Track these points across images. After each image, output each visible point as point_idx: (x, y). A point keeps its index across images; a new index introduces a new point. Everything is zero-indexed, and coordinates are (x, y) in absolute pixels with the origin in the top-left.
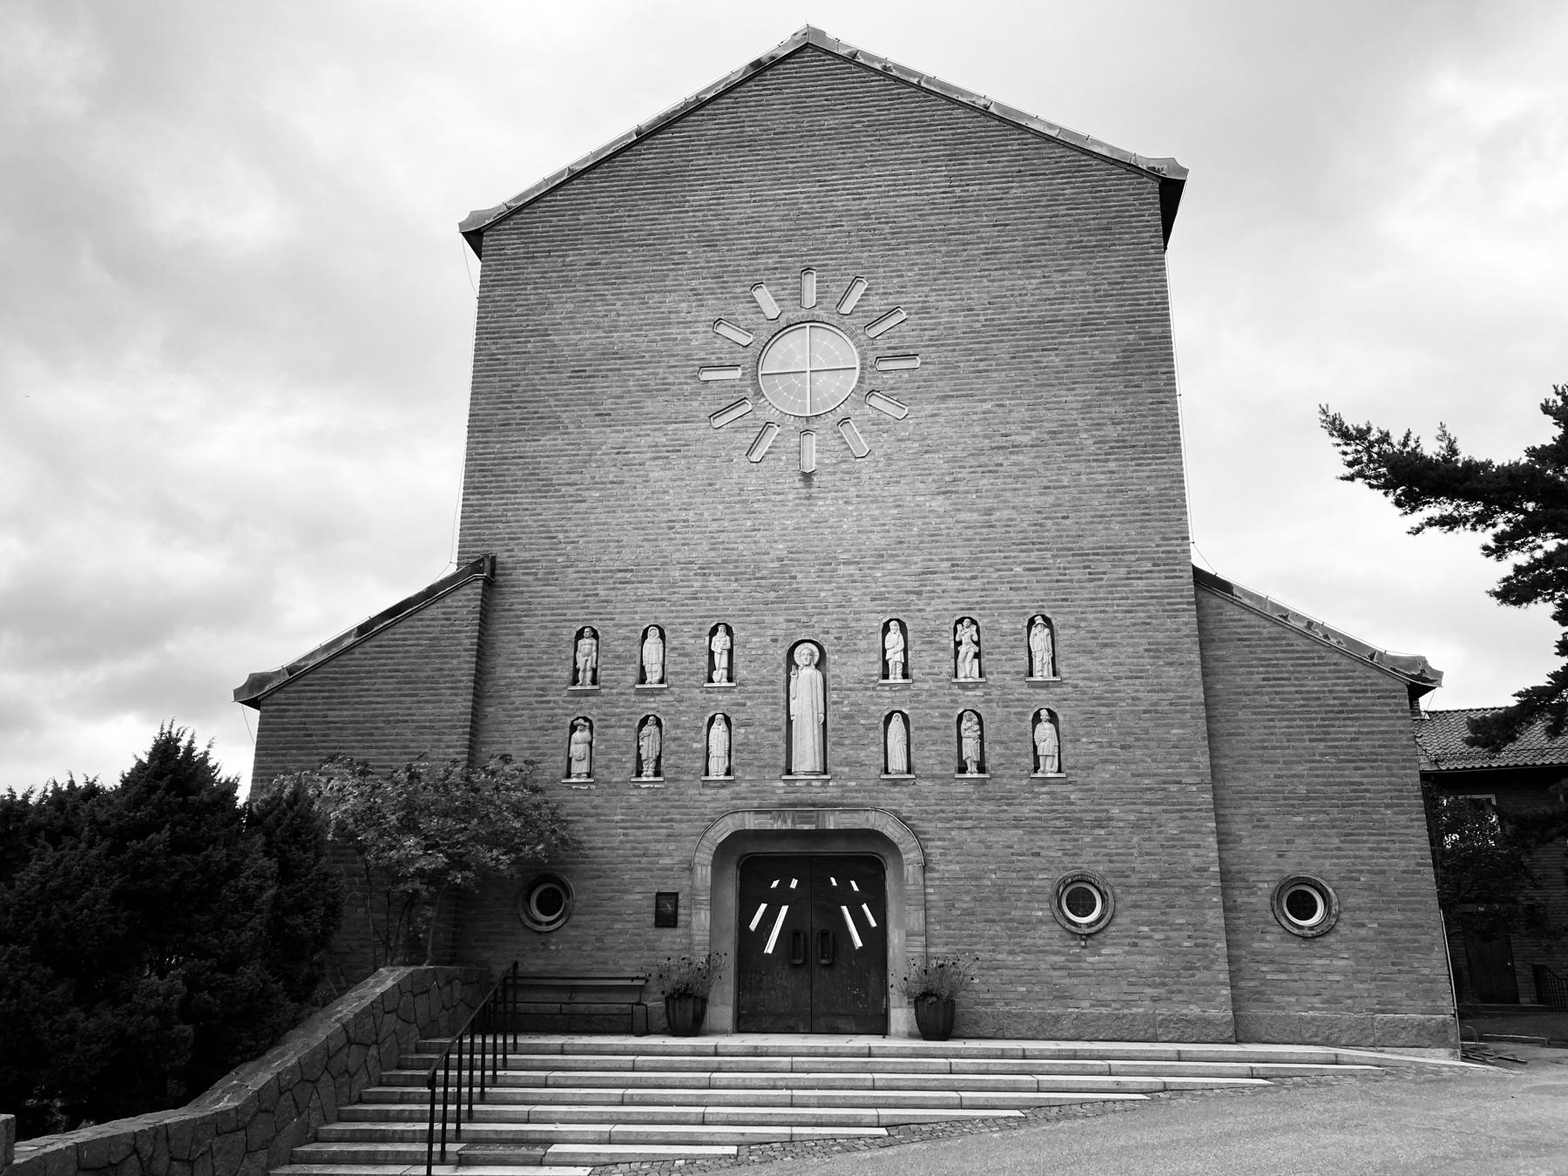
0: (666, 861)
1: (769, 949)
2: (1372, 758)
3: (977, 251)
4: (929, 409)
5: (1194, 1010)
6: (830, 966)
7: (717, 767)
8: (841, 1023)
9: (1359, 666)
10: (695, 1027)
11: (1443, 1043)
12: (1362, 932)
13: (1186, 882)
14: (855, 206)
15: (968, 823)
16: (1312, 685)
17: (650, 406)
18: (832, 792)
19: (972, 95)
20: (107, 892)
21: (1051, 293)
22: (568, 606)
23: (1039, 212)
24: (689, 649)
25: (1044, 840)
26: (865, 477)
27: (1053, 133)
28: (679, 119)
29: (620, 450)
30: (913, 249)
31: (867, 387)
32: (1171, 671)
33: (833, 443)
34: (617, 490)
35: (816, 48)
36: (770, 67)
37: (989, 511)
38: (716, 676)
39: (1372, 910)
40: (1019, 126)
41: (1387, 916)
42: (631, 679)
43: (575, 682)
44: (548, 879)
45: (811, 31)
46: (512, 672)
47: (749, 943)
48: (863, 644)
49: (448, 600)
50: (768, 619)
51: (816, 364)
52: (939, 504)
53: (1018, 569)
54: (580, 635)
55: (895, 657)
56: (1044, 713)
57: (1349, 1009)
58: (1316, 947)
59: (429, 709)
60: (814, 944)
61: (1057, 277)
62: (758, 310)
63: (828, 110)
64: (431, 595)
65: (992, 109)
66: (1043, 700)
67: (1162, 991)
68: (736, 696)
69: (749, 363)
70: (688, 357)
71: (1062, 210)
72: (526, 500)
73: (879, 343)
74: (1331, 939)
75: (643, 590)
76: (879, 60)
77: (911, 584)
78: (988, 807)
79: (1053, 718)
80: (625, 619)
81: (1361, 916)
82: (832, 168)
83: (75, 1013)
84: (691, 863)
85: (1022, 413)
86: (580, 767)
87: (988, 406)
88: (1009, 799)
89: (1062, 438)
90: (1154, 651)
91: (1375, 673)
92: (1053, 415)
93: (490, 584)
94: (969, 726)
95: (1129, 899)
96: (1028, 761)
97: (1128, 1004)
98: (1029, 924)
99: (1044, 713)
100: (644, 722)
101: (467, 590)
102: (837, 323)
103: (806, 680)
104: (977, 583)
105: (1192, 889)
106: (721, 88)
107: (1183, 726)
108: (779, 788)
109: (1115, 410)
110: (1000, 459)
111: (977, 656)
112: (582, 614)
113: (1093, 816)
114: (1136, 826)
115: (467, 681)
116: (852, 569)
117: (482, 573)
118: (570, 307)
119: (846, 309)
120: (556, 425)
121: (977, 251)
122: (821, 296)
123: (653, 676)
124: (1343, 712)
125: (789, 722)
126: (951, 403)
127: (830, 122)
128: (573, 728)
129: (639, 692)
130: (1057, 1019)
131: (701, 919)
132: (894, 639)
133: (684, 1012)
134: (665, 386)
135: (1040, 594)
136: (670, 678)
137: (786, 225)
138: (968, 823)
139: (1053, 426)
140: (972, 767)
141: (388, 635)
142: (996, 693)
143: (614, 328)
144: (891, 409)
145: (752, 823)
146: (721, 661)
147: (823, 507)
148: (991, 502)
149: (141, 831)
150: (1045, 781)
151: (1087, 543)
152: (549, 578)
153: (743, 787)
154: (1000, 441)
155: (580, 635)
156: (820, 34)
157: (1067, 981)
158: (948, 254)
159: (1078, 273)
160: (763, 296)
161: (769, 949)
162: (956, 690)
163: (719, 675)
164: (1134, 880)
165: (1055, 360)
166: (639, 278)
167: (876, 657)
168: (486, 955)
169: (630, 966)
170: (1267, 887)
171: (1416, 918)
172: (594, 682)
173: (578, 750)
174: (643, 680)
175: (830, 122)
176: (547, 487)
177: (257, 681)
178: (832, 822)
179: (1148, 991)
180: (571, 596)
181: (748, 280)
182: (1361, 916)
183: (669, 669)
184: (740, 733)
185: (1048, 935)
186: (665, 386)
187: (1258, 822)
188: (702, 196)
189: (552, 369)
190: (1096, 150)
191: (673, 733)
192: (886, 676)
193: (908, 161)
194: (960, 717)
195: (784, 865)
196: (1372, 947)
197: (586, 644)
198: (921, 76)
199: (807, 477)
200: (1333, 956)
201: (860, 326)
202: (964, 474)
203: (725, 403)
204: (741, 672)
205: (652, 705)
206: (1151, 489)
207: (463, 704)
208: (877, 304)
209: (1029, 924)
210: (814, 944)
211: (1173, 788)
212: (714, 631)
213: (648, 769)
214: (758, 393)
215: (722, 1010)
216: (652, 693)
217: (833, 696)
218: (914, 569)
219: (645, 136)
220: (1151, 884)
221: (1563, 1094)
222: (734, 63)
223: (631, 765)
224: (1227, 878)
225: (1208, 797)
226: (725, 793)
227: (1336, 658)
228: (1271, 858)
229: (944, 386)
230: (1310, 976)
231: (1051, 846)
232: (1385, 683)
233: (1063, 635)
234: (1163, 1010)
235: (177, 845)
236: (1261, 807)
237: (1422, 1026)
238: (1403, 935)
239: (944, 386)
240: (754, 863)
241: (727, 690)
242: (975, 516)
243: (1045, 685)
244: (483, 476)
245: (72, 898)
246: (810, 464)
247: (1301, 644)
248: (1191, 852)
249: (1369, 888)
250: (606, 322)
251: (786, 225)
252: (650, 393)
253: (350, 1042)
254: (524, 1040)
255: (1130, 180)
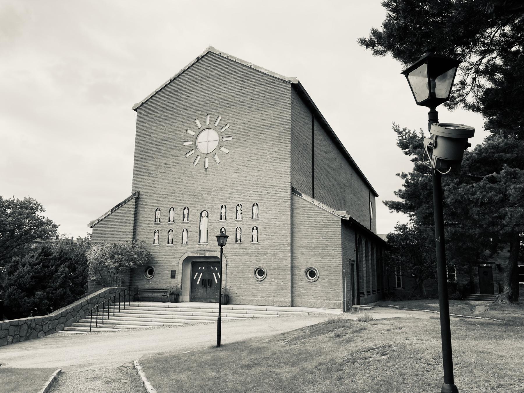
0: (173, 263)
1: (198, 283)
2: (331, 238)
3: (246, 107)
4: (234, 151)
5: (282, 299)
6: (210, 287)
7: (184, 241)
8: (212, 300)
9: (330, 214)
10: (176, 300)
11: (340, 308)
12: (324, 281)
13: (283, 268)
14: (219, 96)
15: (237, 254)
16: (318, 219)
17: (172, 152)
18: (208, 247)
19: (247, 62)
20: (30, 276)
21: (263, 118)
22: (154, 203)
23: (262, 95)
24: (179, 213)
25: (253, 258)
26: (219, 169)
27: (266, 72)
28: (180, 75)
29: (166, 164)
30: (232, 107)
31: (220, 145)
32: (284, 217)
33: (212, 160)
34: (165, 174)
35: (212, 52)
36: (201, 59)
37: (246, 177)
38: (185, 220)
39: (327, 275)
40: (258, 71)
41: (330, 277)
42: (167, 220)
43: (156, 221)
44: (149, 266)
45: (211, 47)
46: (143, 219)
47: (193, 282)
48: (216, 211)
49: (128, 203)
50: (196, 205)
51: (208, 140)
52: (235, 175)
53: (251, 192)
54: (156, 210)
55: (223, 214)
56: (255, 228)
57: (319, 299)
58: (313, 284)
59: (125, 228)
60: (207, 282)
61: (265, 113)
62: (197, 126)
63: (214, 70)
64: (125, 202)
65: (252, 67)
66: (255, 224)
67: (275, 294)
68: (189, 225)
69: (194, 140)
70: (181, 139)
71: (267, 94)
72: (146, 177)
73: (223, 134)
74: (317, 282)
75: (170, 199)
76: (226, 54)
77: (227, 196)
78: (242, 250)
79: (257, 229)
80: (166, 206)
81: (324, 277)
82: (214, 86)
83: (26, 298)
84: (177, 264)
85: (254, 151)
86: (156, 242)
87: (247, 149)
88: (245, 249)
89: (263, 157)
90: (280, 212)
91: (333, 216)
92: (262, 151)
93: (138, 199)
94: (239, 230)
95: (270, 273)
96: (251, 239)
97: (268, 297)
98: (248, 278)
99: (255, 228)
100: (169, 231)
101: (132, 200)
102: (214, 128)
103: (204, 219)
104: (242, 195)
105: (284, 270)
106: (189, 66)
107: (285, 230)
108: (197, 247)
109: (276, 149)
110: (249, 163)
111: (241, 213)
112: (157, 205)
113: (263, 252)
114: (273, 255)
115: (132, 222)
116: (215, 193)
117: (137, 197)
118: (155, 128)
119: (216, 125)
120: (152, 158)
121: (246, 107)
122: (210, 121)
123: (172, 220)
124: (325, 226)
125: (200, 231)
126: (239, 149)
127: (214, 73)
128: (155, 233)
129: (168, 224)
130: (253, 300)
131: (179, 276)
132: (223, 210)
133: (175, 297)
134: (175, 147)
135: (256, 198)
136: (175, 220)
137: (203, 103)
138: (237, 254)
139: (261, 154)
140: (239, 241)
141: (116, 211)
142: (245, 223)
143: (165, 133)
144: (226, 151)
145: (191, 255)
146: (186, 216)
147: (209, 177)
148: (246, 175)
149: (35, 265)
150: (254, 244)
151: (267, 184)
152: (150, 196)
153: (190, 246)
154: (249, 159)
155: (156, 210)
156: (213, 48)
157: (255, 292)
158: (240, 108)
159: (270, 112)
160: (197, 122)
161: (198, 283)
162: (236, 222)
163: (186, 219)
164: (272, 268)
165: (263, 136)
166: (170, 119)
167: (219, 214)
168: (137, 284)
169: (164, 286)
170: (303, 270)
171: (336, 277)
172: (160, 221)
173: (156, 238)
174: (169, 221)
175: (214, 73)
176: (150, 174)
177: (92, 223)
178: (208, 254)
179: (273, 294)
180: (154, 201)
181: (194, 118)
182: (324, 277)
183: (175, 218)
184: (189, 233)
185: (252, 281)
186: (175, 147)
187: (303, 254)
188: (185, 96)
189: (152, 144)
190: (276, 76)
191: (176, 233)
192: (221, 219)
193: (232, 83)
194: (237, 229)
195: (201, 264)
196: (326, 285)
197: (158, 212)
198: (236, 58)
199: (206, 169)
200: (317, 287)
201: (219, 129)
202: (241, 167)
203: (188, 151)
204: (190, 219)
205: (171, 227)
206: (283, 170)
207: (131, 227)
208: (223, 123)
209: (248, 278)
210: (207, 282)
211: (282, 246)
212: (185, 209)
213: (170, 242)
214: (196, 148)
215: (186, 296)
216: (171, 224)
217: (210, 224)
218: (228, 192)
219: (172, 81)
220: (275, 269)
221: (522, 324)
222: (192, 59)
223: (167, 241)
224: (292, 268)
225: (290, 248)
226: (186, 247)
227: (324, 212)
228: (304, 262)
229: (237, 144)
230: (311, 291)
231: (254, 259)
232: (336, 219)
233: (260, 208)
234: (275, 299)
235: (43, 266)
236: (304, 250)
237: (335, 304)
238: (333, 281)
239: (237, 144)
240: (195, 263)
241: (187, 223)
242: (243, 178)
243: (255, 220)
244: (138, 171)
245: (24, 277)
246: (206, 166)
247: (317, 209)
248: (285, 261)
249: (327, 270)
250: (163, 131)
251: (203, 103)
252: (172, 149)
253: (88, 303)
254: (131, 303)
255: (284, 85)
